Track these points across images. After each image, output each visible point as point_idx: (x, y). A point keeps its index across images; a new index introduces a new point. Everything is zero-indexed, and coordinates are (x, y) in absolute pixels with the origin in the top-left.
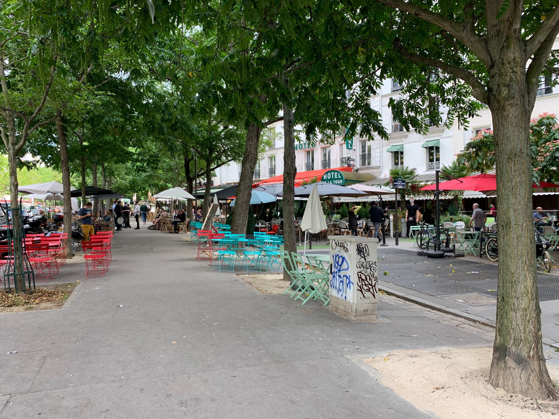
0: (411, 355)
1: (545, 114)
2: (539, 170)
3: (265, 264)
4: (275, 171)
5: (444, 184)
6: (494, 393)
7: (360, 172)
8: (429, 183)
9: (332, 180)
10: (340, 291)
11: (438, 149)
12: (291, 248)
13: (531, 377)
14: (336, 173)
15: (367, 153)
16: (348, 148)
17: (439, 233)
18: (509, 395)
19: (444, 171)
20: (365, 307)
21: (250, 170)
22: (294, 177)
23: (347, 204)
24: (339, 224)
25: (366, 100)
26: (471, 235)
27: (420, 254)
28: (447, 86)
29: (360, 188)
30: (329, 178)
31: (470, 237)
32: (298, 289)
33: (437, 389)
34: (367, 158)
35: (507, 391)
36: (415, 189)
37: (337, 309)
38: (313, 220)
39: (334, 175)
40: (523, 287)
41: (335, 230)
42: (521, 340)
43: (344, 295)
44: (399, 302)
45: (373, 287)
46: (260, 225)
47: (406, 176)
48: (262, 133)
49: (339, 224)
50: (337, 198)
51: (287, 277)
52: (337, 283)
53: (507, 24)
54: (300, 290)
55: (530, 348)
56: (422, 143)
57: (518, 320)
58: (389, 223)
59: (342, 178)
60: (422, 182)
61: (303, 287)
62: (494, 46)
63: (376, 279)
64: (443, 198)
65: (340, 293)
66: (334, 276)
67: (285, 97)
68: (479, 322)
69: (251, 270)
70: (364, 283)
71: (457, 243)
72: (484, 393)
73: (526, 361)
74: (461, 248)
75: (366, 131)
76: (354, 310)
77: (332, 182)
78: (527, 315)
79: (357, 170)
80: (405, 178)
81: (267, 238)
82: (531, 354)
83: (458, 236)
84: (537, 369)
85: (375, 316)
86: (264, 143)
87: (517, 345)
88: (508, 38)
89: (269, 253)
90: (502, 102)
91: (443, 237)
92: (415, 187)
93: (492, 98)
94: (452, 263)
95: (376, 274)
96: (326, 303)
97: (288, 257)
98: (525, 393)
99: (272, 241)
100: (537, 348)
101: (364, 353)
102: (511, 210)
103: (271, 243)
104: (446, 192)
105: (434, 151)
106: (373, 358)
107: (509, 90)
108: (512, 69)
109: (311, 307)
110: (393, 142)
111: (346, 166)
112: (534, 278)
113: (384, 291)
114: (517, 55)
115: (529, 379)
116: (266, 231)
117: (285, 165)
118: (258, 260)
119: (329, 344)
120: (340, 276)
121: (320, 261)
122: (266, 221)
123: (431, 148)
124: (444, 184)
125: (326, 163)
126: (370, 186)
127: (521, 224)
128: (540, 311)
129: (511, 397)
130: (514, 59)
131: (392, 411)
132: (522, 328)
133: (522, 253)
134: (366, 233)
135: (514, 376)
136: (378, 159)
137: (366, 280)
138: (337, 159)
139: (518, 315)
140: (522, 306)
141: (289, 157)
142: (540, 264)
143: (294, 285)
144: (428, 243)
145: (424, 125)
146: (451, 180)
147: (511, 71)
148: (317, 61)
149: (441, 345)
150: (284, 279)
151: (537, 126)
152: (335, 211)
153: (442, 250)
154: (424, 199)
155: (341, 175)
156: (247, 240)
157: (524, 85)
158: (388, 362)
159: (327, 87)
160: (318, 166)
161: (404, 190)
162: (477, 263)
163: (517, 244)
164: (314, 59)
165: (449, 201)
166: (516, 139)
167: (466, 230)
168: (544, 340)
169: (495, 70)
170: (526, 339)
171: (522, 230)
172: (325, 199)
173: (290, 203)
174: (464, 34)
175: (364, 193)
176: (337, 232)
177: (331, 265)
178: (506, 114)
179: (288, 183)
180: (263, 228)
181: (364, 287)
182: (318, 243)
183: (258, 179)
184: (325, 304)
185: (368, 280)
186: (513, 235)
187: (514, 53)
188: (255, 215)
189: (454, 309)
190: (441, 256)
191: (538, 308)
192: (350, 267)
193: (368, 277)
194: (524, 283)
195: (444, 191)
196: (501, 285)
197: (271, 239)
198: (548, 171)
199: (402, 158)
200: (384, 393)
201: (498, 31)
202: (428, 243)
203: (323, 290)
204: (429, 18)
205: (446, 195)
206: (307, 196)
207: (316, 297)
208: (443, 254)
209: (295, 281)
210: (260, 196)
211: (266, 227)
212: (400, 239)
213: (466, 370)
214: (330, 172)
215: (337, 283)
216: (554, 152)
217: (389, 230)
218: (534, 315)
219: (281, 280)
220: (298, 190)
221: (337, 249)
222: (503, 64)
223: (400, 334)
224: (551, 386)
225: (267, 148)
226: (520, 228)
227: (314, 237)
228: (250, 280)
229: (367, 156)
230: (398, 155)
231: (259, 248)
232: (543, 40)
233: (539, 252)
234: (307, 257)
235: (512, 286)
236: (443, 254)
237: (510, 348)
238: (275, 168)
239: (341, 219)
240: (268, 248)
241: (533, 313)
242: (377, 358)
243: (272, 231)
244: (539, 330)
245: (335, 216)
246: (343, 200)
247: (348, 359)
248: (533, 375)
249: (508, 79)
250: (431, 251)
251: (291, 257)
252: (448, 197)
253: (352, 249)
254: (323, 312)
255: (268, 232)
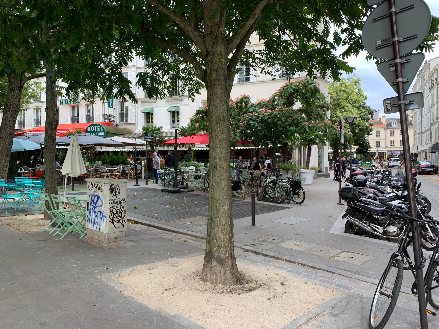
0: (149, 268)
1: (244, 95)
2: (240, 132)
3: (27, 206)
4: (40, 121)
5: (182, 139)
6: (204, 286)
7: (119, 127)
8: (171, 138)
9: (95, 132)
10: (95, 224)
11: (178, 113)
12: (52, 190)
13: (227, 271)
14: (98, 127)
15: (125, 112)
16: (109, 107)
17: (177, 175)
18: (213, 286)
19: (181, 129)
20: (115, 235)
21: (11, 119)
22: (56, 128)
23: (108, 152)
24: (100, 169)
25: (120, 68)
26: (198, 176)
27: (163, 191)
28: (182, 66)
29: (118, 139)
30: (92, 130)
31: (197, 177)
32: (58, 226)
33: (166, 290)
34: (125, 116)
35: (212, 283)
36: (161, 142)
37: (92, 239)
38: (73, 165)
39: (97, 128)
40: (223, 210)
41: (97, 174)
42: (221, 247)
43: (98, 226)
44: (144, 228)
45: (122, 218)
46: (23, 170)
47: (154, 132)
48: (25, 86)
49: (100, 169)
50: (99, 147)
51: (47, 217)
52: (92, 218)
53: (217, 27)
54: (59, 227)
55: (227, 251)
56: (167, 108)
57: (220, 234)
58: (142, 168)
59: (104, 131)
60: (166, 137)
61: (62, 224)
62: (209, 41)
63: (125, 212)
64: (181, 149)
65: (95, 226)
66: (90, 212)
67: (45, 56)
68: (199, 237)
69: (11, 212)
70: (115, 216)
71: (189, 181)
72: (198, 288)
73: (224, 261)
74: (192, 185)
75: (120, 94)
76: (106, 238)
77: (95, 134)
78: (225, 229)
79: (117, 125)
80: (154, 133)
81: (29, 182)
82: (227, 256)
83: (190, 177)
84: (230, 265)
85: (123, 241)
86: (28, 95)
87: (218, 250)
88: (217, 37)
89: (30, 196)
90: (213, 82)
91: (179, 178)
92: (161, 140)
93: (207, 78)
94: (186, 197)
95: (125, 208)
96: (83, 235)
97: (48, 198)
98: (223, 283)
99: (33, 185)
100: (231, 250)
101: (112, 272)
102: (217, 157)
103: (33, 187)
104: (183, 145)
105: (176, 115)
106: (119, 275)
107: (217, 74)
108: (219, 59)
109: (69, 239)
110: (146, 105)
111: (107, 121)
112: (230, 203)
113: (133, 221)
114: (222, 50)
115: (225, 272)
116: (29, 176)
117: (46, 116)
118: (18, 203)
119: (82, 269)
120: (95, 212)
121: (79, 201)
122: (30, 167)
123: (173, 112)
124: (182, 139)
125: (90, 118)
126: (127, 139)
127: (223, 167)
128: (233, 226)
129: (215, 287)
130: (221, 52)
131: (130, 314)
132: (222, 238)
133: (223, 187)
134: (122, 176)
135: (217, 272)
136: (134, 117)
137: (117, 213)
138: (99, 115)
139: (220, 229)
140: (223, 223)
141: (51, 109)
142: (239, 194)
143: (54, 223)
144: (169, 182)
145: (163, 93)
146: (186, 136)
147: (218, 61)
148: (76, 28)
149: (172, 257)
150: (45, 218)
151: (239, 102)
152: (98, 158)
153: (179, 187)
154: (168, 149)
155: (103, 128)
156: (6, 185)
157: (227, 72)
158: (131, 276)
159: (85, 52)
160: (83, 119)
161: (153, 143)
162: (202, 195)
163: (220, 180)
164: (74, 26)
165: (185, 152)
166: (221, 109)
167: (196, 173)
168: (235, 244)
169: (209, 58)
170: (224, 245)
171: (223, 171)
172: (89, 148)
173: (51, 150)
174: (189, 29)
175: (121, 144)
176: (98, 176)
177: (88, 203)
178: (215, 91)
179: (50, 132)
180: (26, 173)
181: (115, 219)
182: (81, 185)
183: (23, 128)
184: (82, 236)
185: (119, 213)
186: (218, 175)
187: (221, 49)
188: (18, 162)
189: (184, 229)
190: (178, 192)
191: (232, 223)
192: (103, 204)
193: (118, 211)
194: (224, 206)
195: (181, 144)
196: (210, 210)
197: (33, 183)
198: (246, 133)
199: (152, 118)
200: (125, 301)
201: (211, 31)
202: (169, 182)
203: (81, 224)
204: (166, 12)
205: (183, 147)
206: (68, 145)
207: (74, 231)
208: (179, 190)
209: (55, 219)
210: (22, 144)
211: (29, 173)
212: (149, 180)
213: (187, 273)
214: (94, 125)
215: (92, 218)
216: (249, 121)
217: (141, 173)
218: (229, 229)
219: (41, 219)
220: (59, 139)
221: (93, 190)
222: (214, 55)
223: (142, 253)
224: (239, 276)
225: (32, 100)
226: (222, 170)
227: (77, 180)
228: (8, 221)
229: (125, 114)
230: (149, 116)
231: (20, 191)
232: (238, 43)
233: (236, 186)
234: (67, 197)
235: (217, 210)
236: (179, 190)
237: (214, 253)
238: (41, 119)
239: (102, 165)
240: (30, 190)
241: (228, 227)
242: (122, 274)
243: (36, 176)
244: (232, 238)
245: (97, 162)
246: (105, 149)
247: (98, 279)
248: (228, 269)
249: (217, 66)
250: (171, 188)
251: (51, 198)
252: (184, 149)
253: (106, 189)
254: (79, 243)
255: (30, 177)
